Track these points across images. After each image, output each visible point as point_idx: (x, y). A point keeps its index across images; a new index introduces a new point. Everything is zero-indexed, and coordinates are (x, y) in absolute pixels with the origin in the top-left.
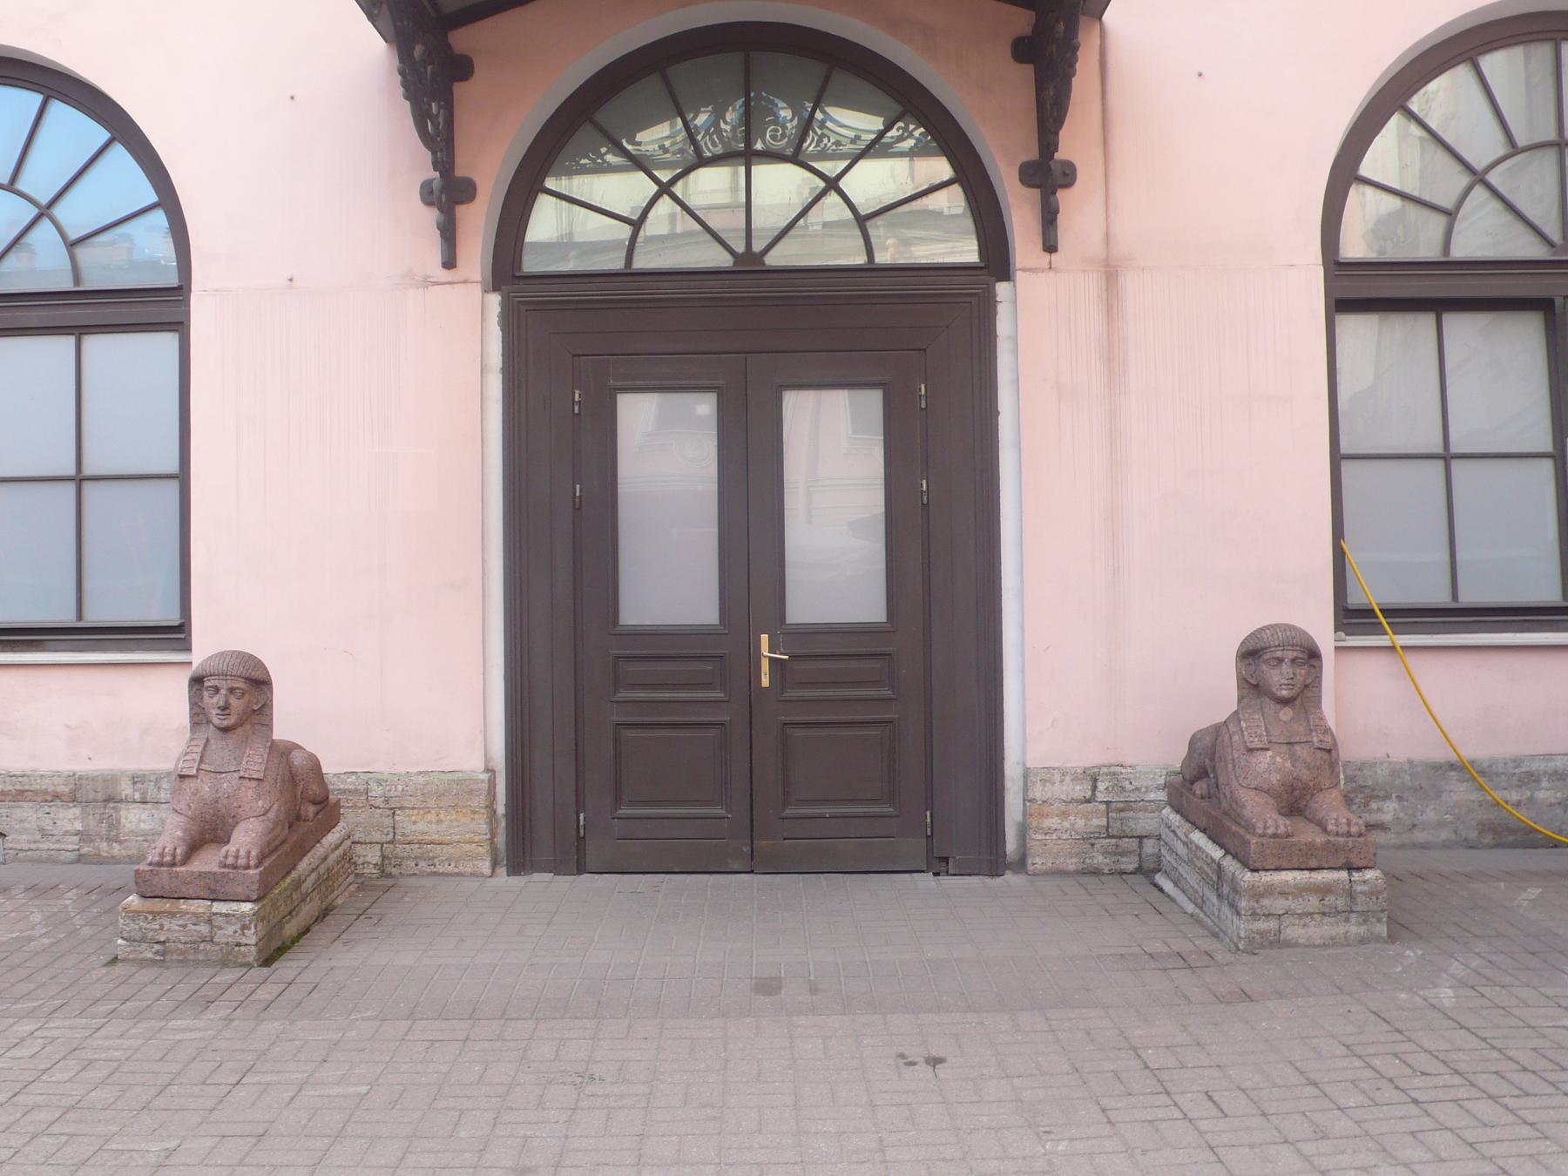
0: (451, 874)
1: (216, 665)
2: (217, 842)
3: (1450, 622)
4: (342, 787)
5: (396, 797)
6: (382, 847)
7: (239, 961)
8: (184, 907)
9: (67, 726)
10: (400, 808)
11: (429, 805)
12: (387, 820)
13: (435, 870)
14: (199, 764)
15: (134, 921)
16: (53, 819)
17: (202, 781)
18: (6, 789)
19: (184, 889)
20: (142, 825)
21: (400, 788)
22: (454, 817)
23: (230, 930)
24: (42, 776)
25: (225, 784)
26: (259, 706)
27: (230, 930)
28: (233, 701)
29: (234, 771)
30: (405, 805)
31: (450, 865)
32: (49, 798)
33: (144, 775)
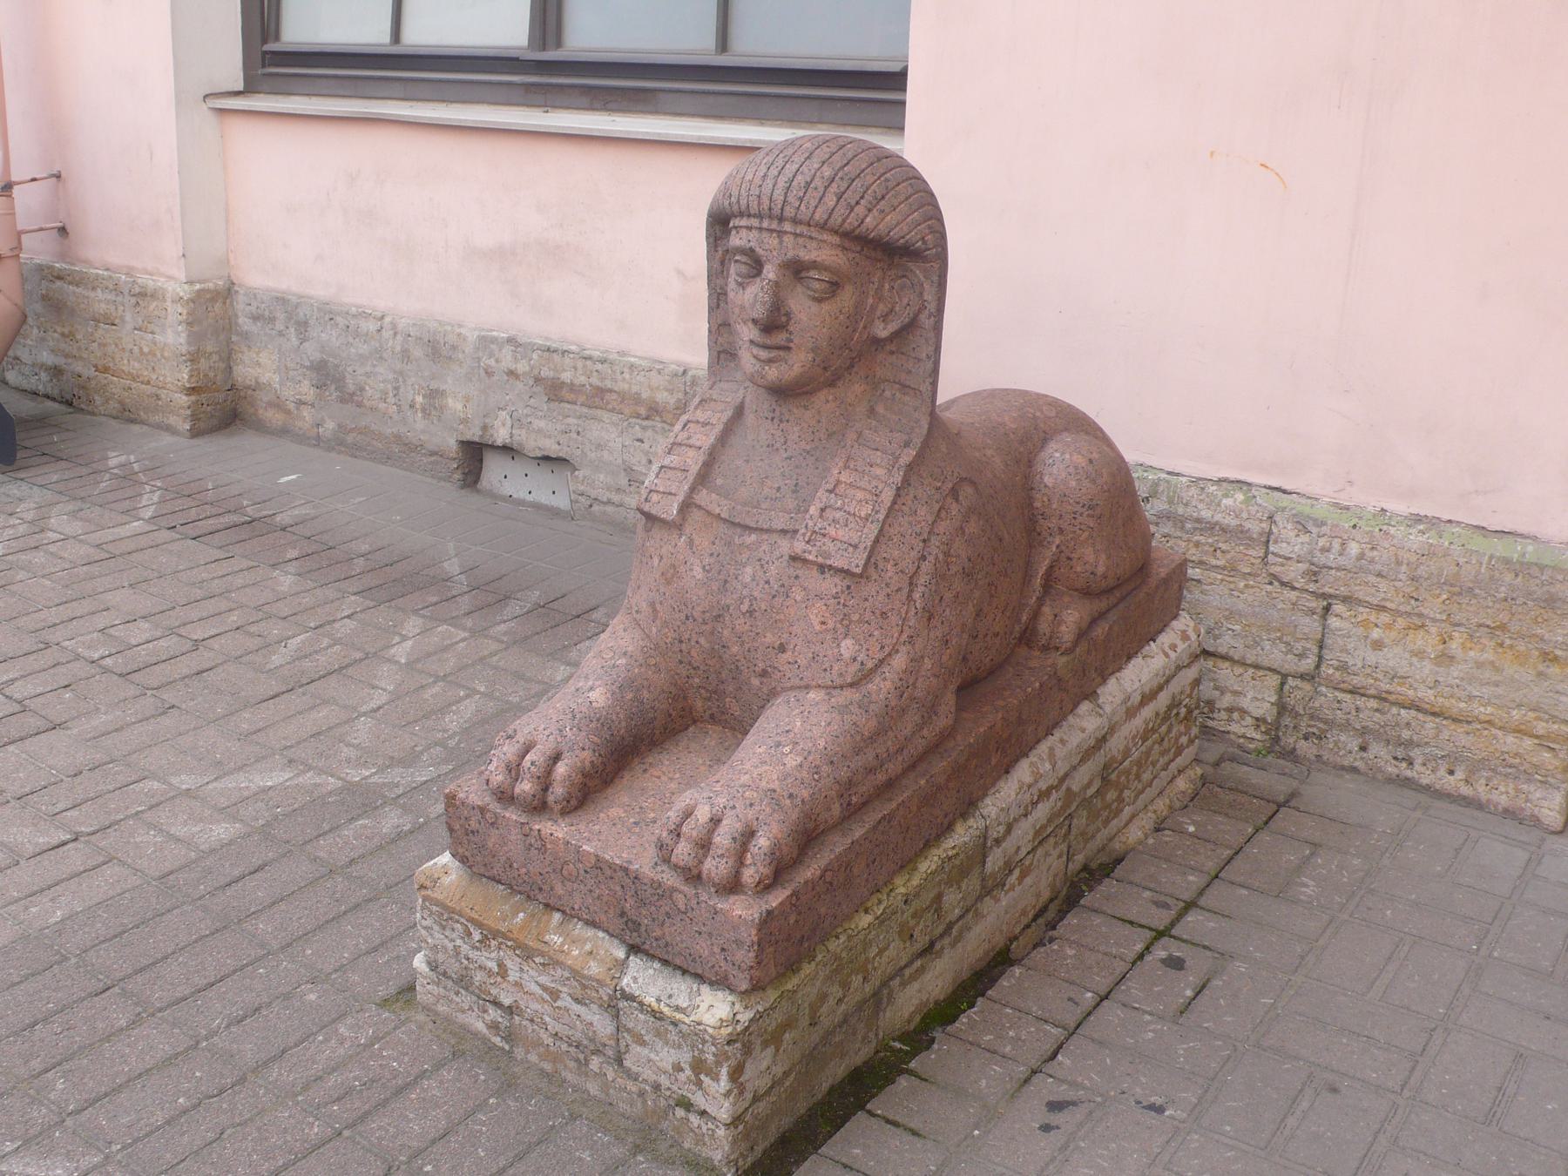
0: (1449, 795)
1: (758, 181)
2: (725, 725)
3: (423, 80)
4: (1206, 514)
5: (1338, 569)
6: (1283, 684)
7: (686, 1145)
8: (556, 939)
9: (680, 273)
10: (1346, 600)
11: (1425, 612)
12: (1307, 620)
13: (1409, 773)
14: (693, 489)
15: (444, 928)
16: (647, 453)
17: (691, 542)
18: (577, 382)
19: (559, 890)
21: (1354, 549)
22: (1489, 655)
23: (666, 1056)
24: (632, 367)
25: (749, 570)
26: (893, 326)
27: (666, 1056)
28: (803, 309)
29: (784, 532)
30: (1361, 595)
31: (1451, 772)
32: (643, 411)
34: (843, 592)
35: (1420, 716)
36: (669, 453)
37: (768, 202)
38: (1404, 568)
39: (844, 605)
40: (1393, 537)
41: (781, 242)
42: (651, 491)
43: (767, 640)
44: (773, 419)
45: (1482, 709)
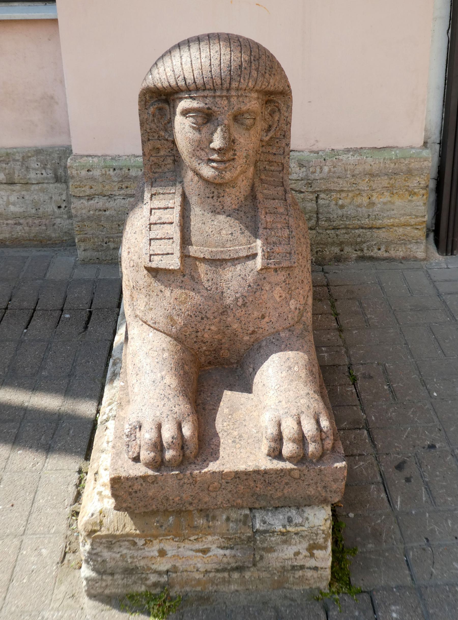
5: (320, 179)
12: (310, 204)
20: (12, 208)
21: (326, 169)
31: (379, 249)
33: (7, 154)
34: (287, 277)
35: (364, 231)
36: (150, 230)
37: (220, 81)
38: (349, 172)
39: (289, 284)
40: (342, 160)
41: (229, 102)
42: (151, 255)
43: (255, 315)
44: (212, 197)
45: (388, 221)
